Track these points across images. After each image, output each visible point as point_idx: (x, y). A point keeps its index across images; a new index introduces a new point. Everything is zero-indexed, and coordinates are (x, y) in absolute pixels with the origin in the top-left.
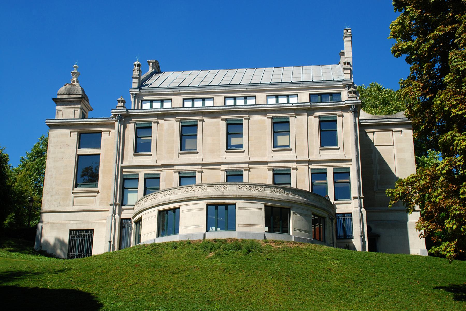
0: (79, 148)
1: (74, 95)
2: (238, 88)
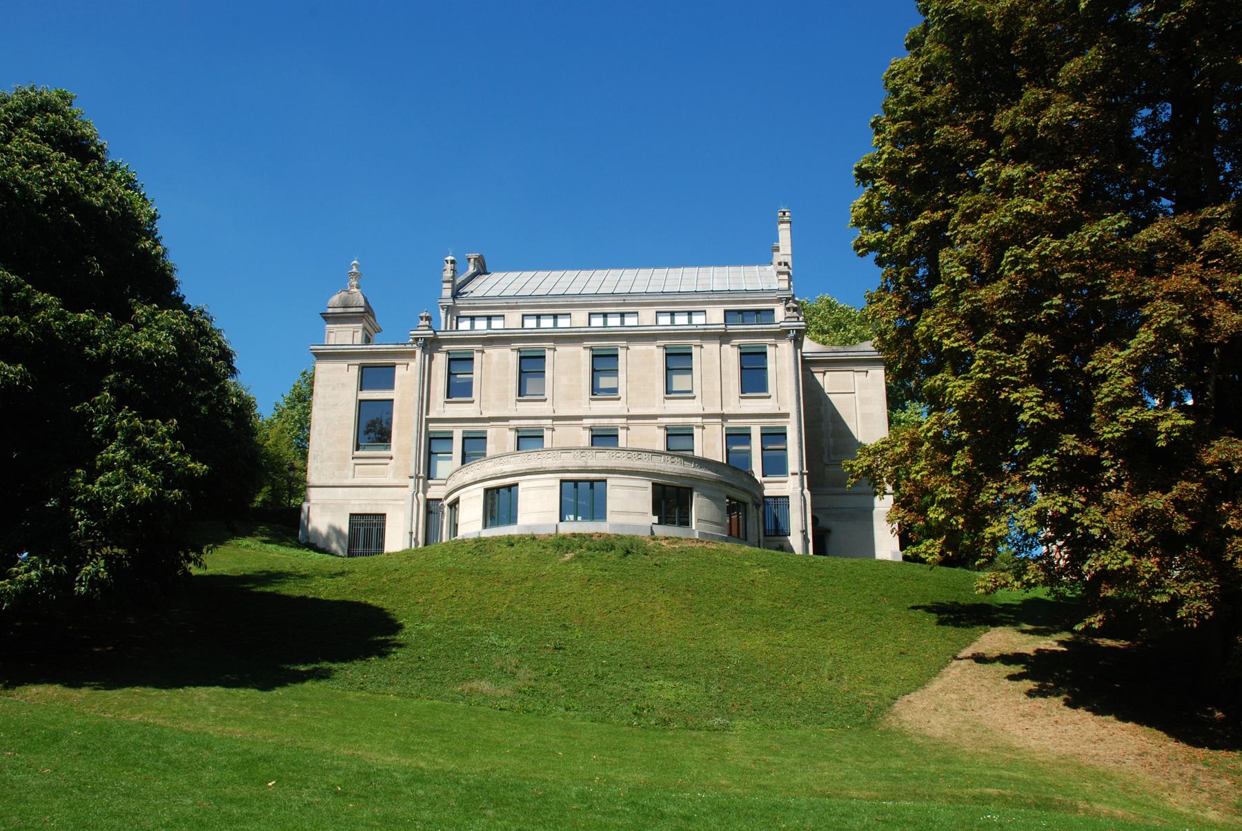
0: (361, 390)
2: (610, 300)
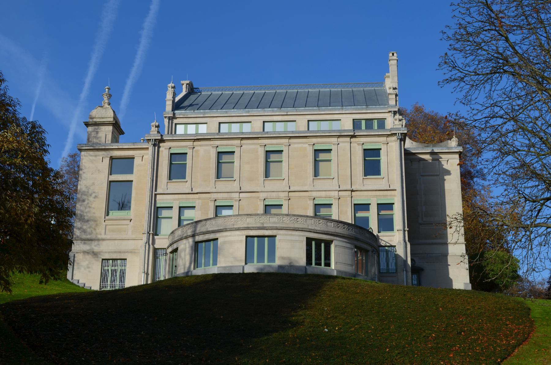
0: (111, 175)
1: (106, 118)
